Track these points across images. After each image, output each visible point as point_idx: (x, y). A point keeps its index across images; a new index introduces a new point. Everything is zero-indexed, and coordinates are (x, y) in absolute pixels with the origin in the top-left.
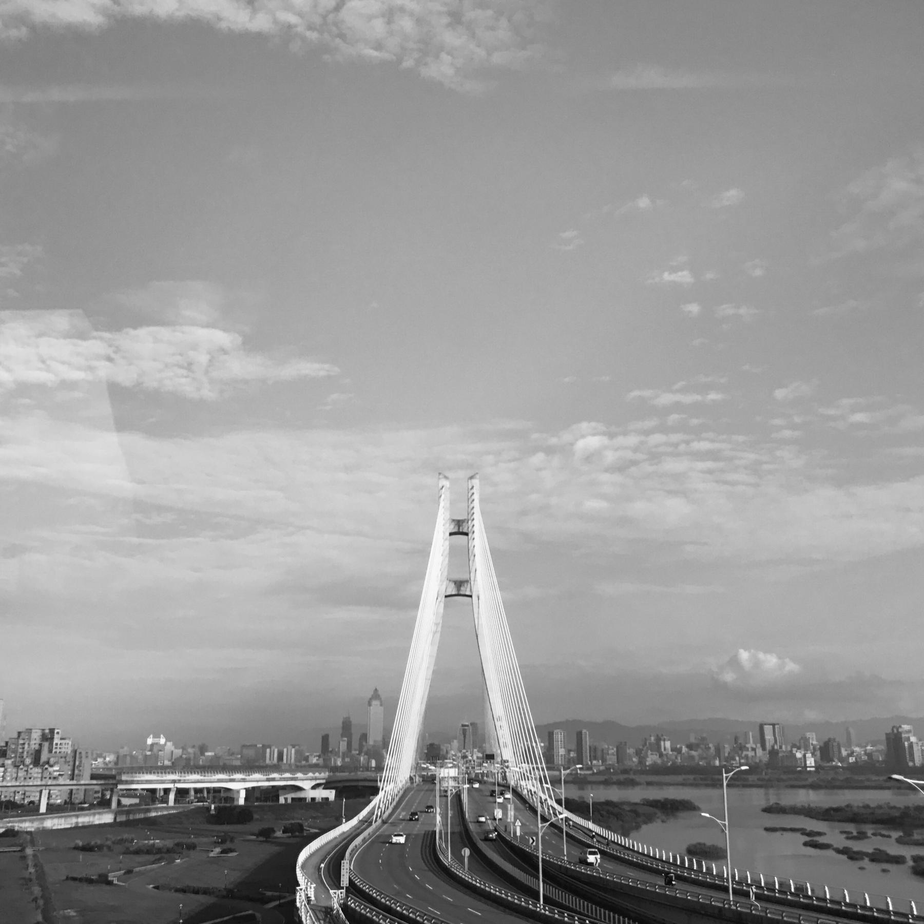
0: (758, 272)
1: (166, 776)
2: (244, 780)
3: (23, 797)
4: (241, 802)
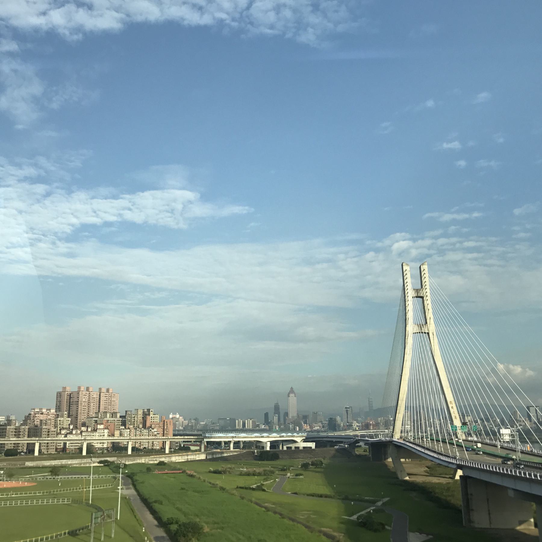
0: (501, 140)
1: (217, 435)
2: (268, 437)
3: (140, 445)
4: (268, 449)
